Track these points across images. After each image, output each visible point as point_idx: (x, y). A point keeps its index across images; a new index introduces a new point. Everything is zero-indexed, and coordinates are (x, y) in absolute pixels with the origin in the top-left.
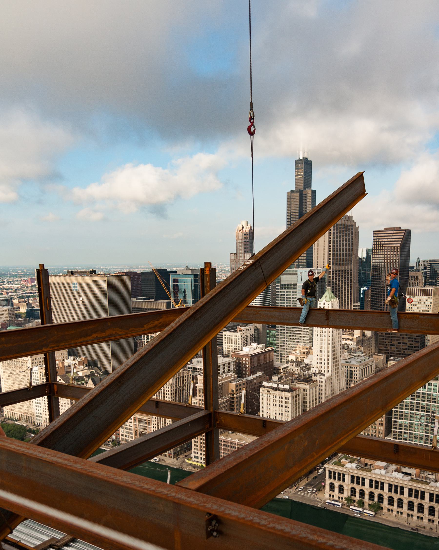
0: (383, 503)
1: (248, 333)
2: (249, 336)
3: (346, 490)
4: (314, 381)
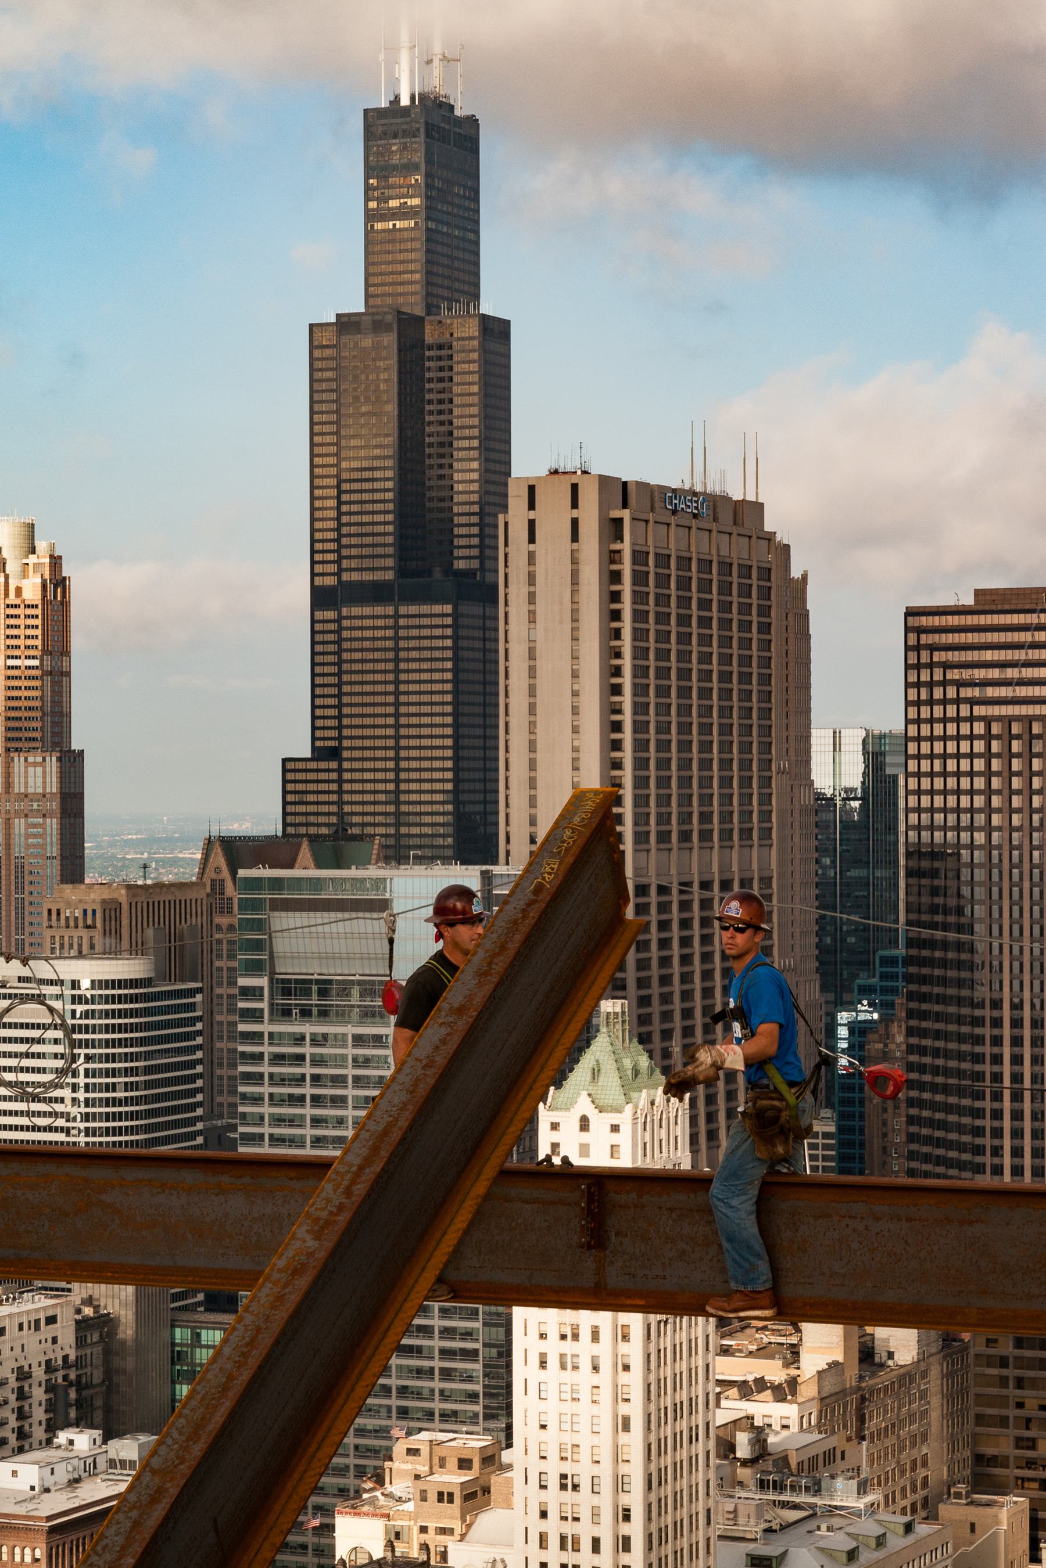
2: (39, 1374)
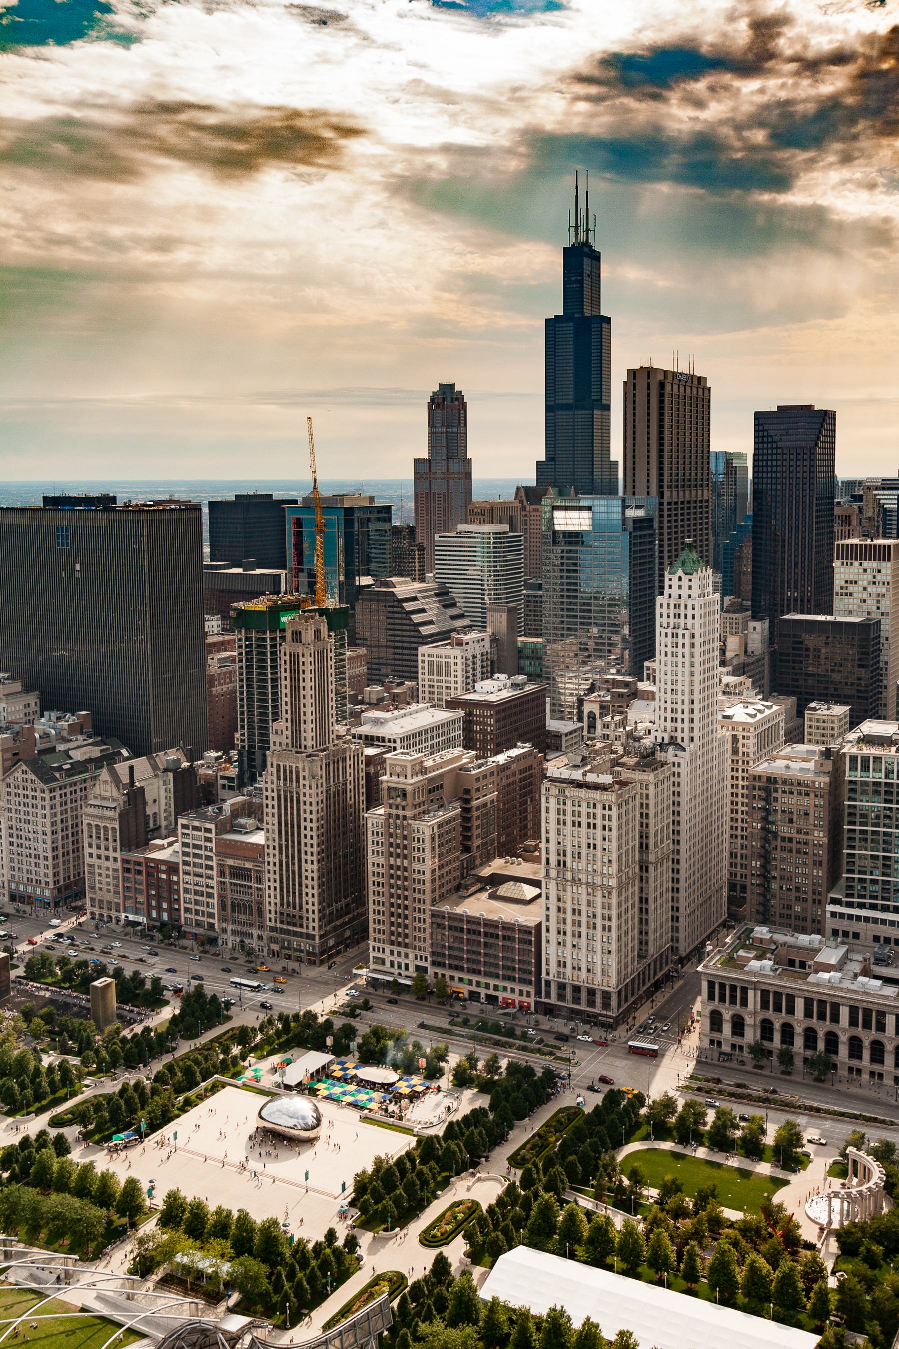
0: (836, 1053)
1: (478, 649)
2: (479, 656)
3: (749, 1025)
4: (663, 764)
